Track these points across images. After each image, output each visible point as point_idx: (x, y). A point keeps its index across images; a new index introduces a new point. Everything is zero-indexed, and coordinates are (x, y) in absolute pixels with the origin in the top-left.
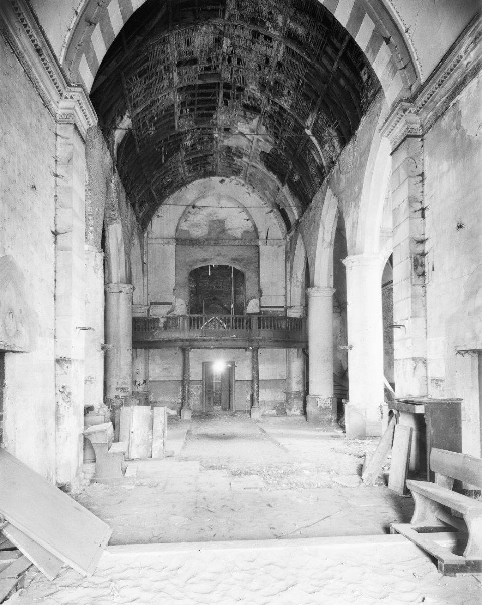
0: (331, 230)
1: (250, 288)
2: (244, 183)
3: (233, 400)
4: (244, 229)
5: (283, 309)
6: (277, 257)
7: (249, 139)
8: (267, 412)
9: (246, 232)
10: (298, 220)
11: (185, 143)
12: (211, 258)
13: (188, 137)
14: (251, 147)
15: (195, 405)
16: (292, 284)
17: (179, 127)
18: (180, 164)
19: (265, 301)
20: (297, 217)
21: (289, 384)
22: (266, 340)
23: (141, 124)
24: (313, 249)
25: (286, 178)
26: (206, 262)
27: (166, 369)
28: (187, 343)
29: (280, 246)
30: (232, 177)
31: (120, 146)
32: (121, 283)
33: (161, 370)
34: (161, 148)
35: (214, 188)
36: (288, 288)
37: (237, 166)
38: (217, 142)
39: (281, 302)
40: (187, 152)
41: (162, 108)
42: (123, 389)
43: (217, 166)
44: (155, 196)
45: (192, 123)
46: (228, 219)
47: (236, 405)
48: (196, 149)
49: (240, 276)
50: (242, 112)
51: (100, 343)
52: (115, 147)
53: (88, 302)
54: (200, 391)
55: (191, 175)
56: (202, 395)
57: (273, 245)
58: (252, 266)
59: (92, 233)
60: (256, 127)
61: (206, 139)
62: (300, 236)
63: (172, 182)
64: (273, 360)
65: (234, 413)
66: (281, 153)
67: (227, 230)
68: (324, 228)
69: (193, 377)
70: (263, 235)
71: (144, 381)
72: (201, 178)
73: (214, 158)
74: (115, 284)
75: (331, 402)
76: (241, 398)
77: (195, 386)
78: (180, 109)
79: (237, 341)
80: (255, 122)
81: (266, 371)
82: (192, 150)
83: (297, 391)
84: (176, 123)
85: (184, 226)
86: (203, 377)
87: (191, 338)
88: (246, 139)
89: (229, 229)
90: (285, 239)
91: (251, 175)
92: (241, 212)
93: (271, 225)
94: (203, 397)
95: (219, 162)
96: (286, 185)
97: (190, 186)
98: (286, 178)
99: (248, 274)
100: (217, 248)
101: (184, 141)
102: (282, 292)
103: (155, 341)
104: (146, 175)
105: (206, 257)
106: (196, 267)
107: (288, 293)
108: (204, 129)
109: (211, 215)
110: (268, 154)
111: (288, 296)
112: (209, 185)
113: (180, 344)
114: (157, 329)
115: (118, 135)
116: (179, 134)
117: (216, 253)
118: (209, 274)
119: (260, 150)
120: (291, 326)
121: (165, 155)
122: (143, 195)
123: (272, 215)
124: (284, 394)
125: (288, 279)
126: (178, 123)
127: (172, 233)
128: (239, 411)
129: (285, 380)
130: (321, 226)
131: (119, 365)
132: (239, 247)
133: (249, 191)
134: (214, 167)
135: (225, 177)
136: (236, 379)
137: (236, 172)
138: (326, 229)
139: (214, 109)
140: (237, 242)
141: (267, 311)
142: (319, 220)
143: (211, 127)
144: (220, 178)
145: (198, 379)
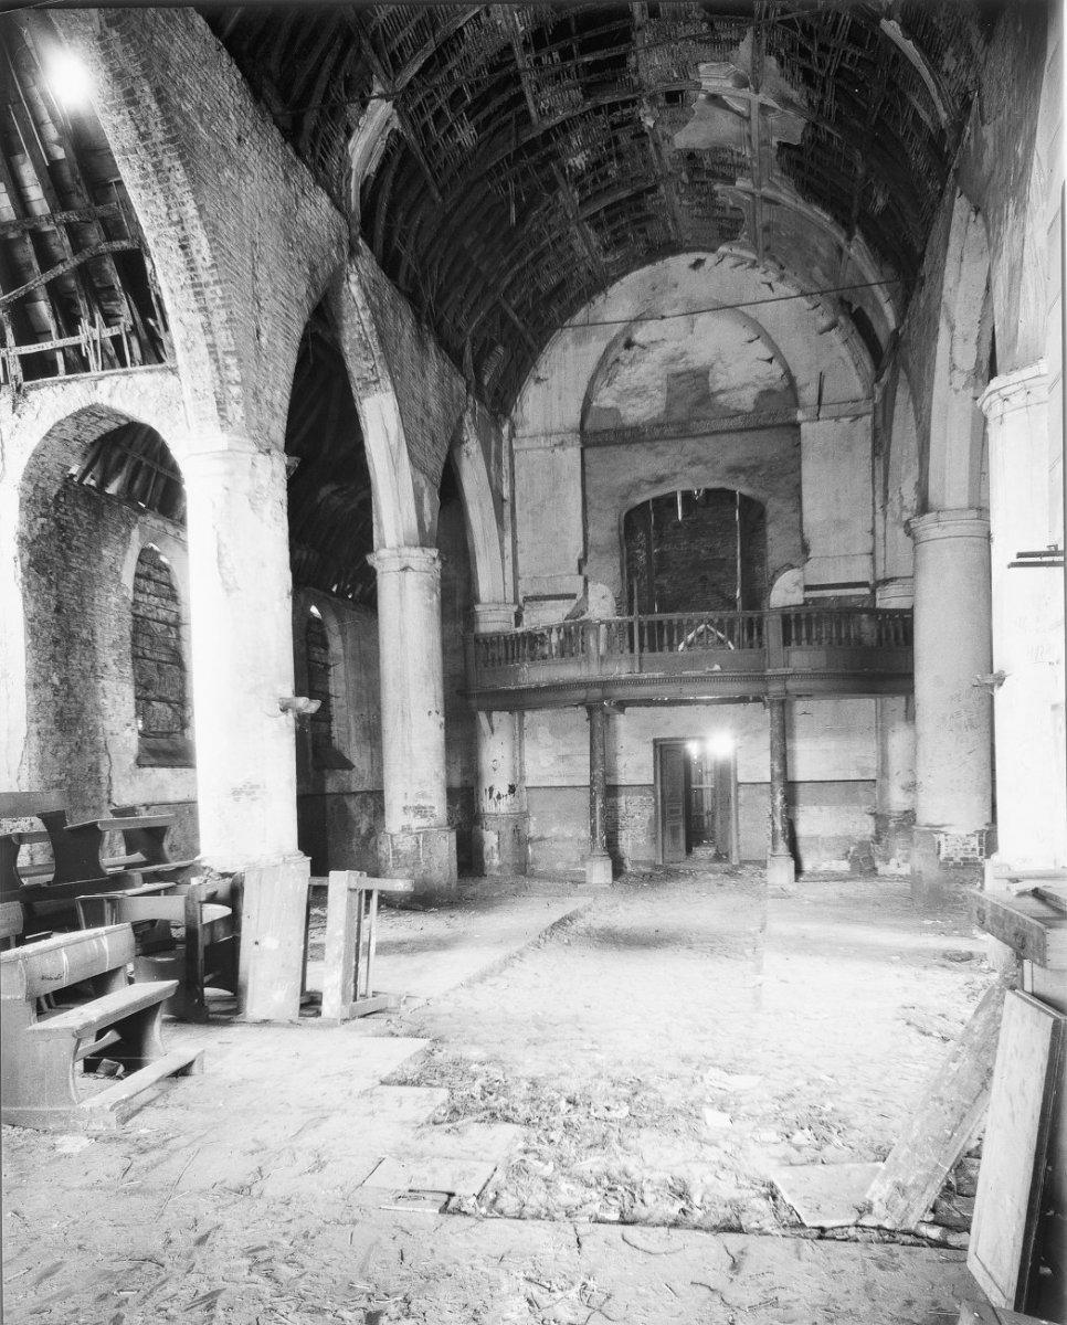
0: (976, 331)
1: (777, 543)
2: (753, 257)
3: (734, 834)
4: (762, 387)
5: (866, 591)
6: (849, 448)
7: (738, 113)
8: (824, 866)
9: (767, 393)
10: (896, 331)
11: (571, 161)
12: (675, 474)
13: (574, 143)
14: (749, 137)
15: (635, 847)
16: (889, 519)
17: (541, 114)
18: (573, 229)
19: (819, 571)
20: (892, 325)
21: (884, 792)
22: (804, 676)
23: (429, 117)
24: (926, 400)
25: (855, 213)
26: (661, 486)
27: (564, 758)
28: (597, 692)
29: (857, 417)
30: (723, 249)
31: (371, 189)
32: (407, 544)
33: (552, 761)
34: (506, 188)
35: (676, 286)
36: (879, 532)
37: (728, 211)
38: (656, 145)
39: (860, 571)
40: (582, 189)
41: (480, 61)
42: (420, 811)
43: (674, 220)
44: (521, 326)
45: (577, 95)
46: (719, 365)
47: (742, 848)
48: (605, 176)
49: (754, 514)
50: (705, 26)
51: (274, 695)
52: (354, 185)
53: (239, 589)
54: (649, 812)
55: (610, 259)
56: (653, 822)
57: (837, 418)
58: (783, 482)
59: (237, 403)
60: (749, 68)
61: (625, 139)
62: (902, 376)
63: (562, 284)
64: (843, 729)
65: (736, 868)
66: (829, 134)
67: (715, 394)
68: (952, 328)
69: (624, 777)
70: (808, 394)
71: (512, 789)
72: (643, 265)
73: (662, 197)
74: (394, 548)
75: (980, 843)
76: (752, 827)
77: (637, 799)
78: (531, 56)
79: (722, 679)
80: (745, 50)
81: (813, 758)
82: (594, 181)
83: (906, 812)
84: (531, 104)
85: (605, 398)
86: (655, 778)
87: (605, 679)
88: (731, 116)
89: (722, 391)
90: (871, 397)
91: (766, 229)
92: (752, 341)
93: (846, 372)
94: (656, 826)
95: (675, 201)
96: (858, 236)
97: (615, 290)
98: (855, 213)
99: (773, 506)
100: (690, 444)
101: (568, 156)
102: (863, 544)
103: (520, 690)
104: (483, 268)
105: (661, 473)
106: (639, 500)
107: (880, 543)
108: (613, 107)
109: (673, 360)
110: (798, 148)
111: (880, 553)
112: (665, 282)
113: (581, 694)
114: (524, 660)
115: (364, 144)
116: (547, 137)
117: (688, 459)
118: (680, 518)
119: (774, 141)
120: (888, 632)
121: (518, 200)
122: (484, 323)
123: (835, 337)
124: (871, 820)
125: (878, 506)
126: (536, 103)
127: (573, 416)
128: (747, 862)
129: (874, 781)
130: (943, 325)
131: (407, 749)
132: (747, 434)
133: (769, 281)
134: (670, 224)
135: (704, 250)
136: (740, 780)
137: (728, 230)
138: (959, 329)
139: (625, 36)
140: (738, 422)
141: (824, 599)
142: (939, 307)
143: (629, 97)
144: (691, 257)
145: (642, 783)
